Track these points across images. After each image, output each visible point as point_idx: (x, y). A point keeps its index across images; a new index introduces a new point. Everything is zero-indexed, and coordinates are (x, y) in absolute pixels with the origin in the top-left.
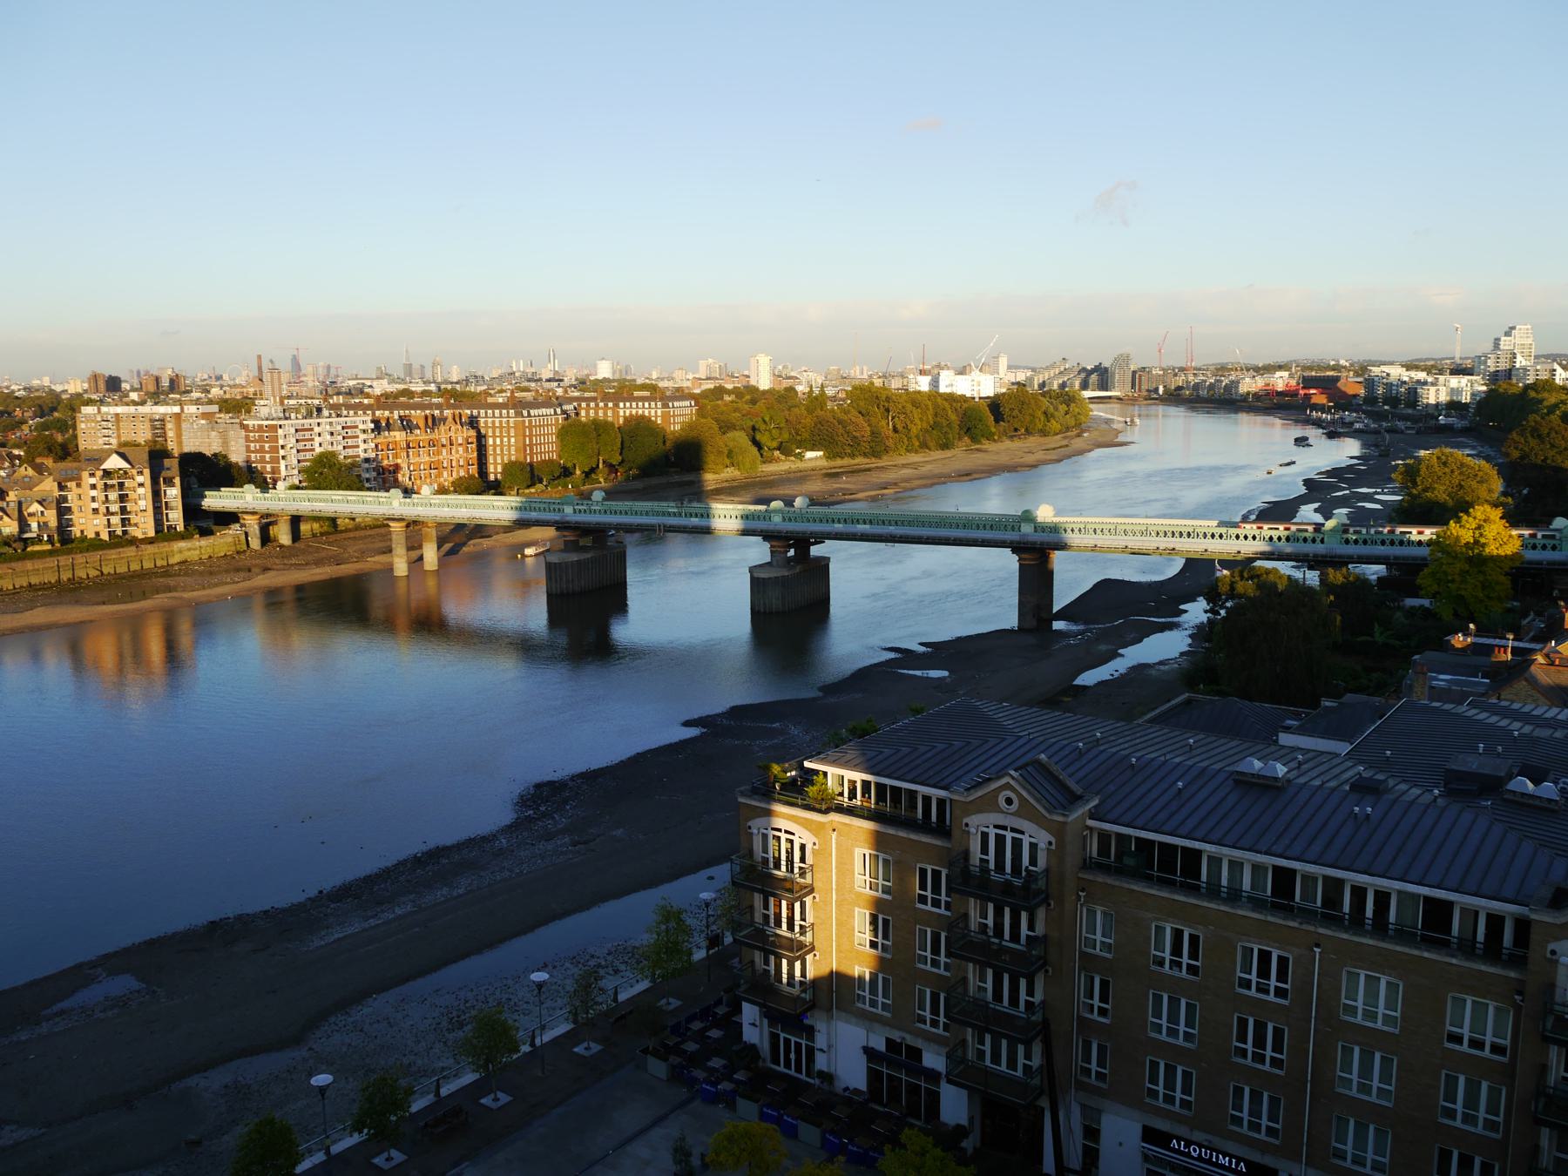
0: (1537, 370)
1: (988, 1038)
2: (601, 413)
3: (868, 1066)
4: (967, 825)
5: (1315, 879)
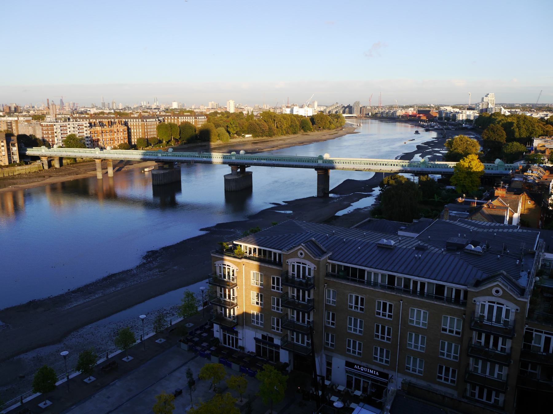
0: (496, 109)
1: (295, 333)
2: (172, 121)
3: (256, 344)
4: (287, 262)
5: (424, 283)
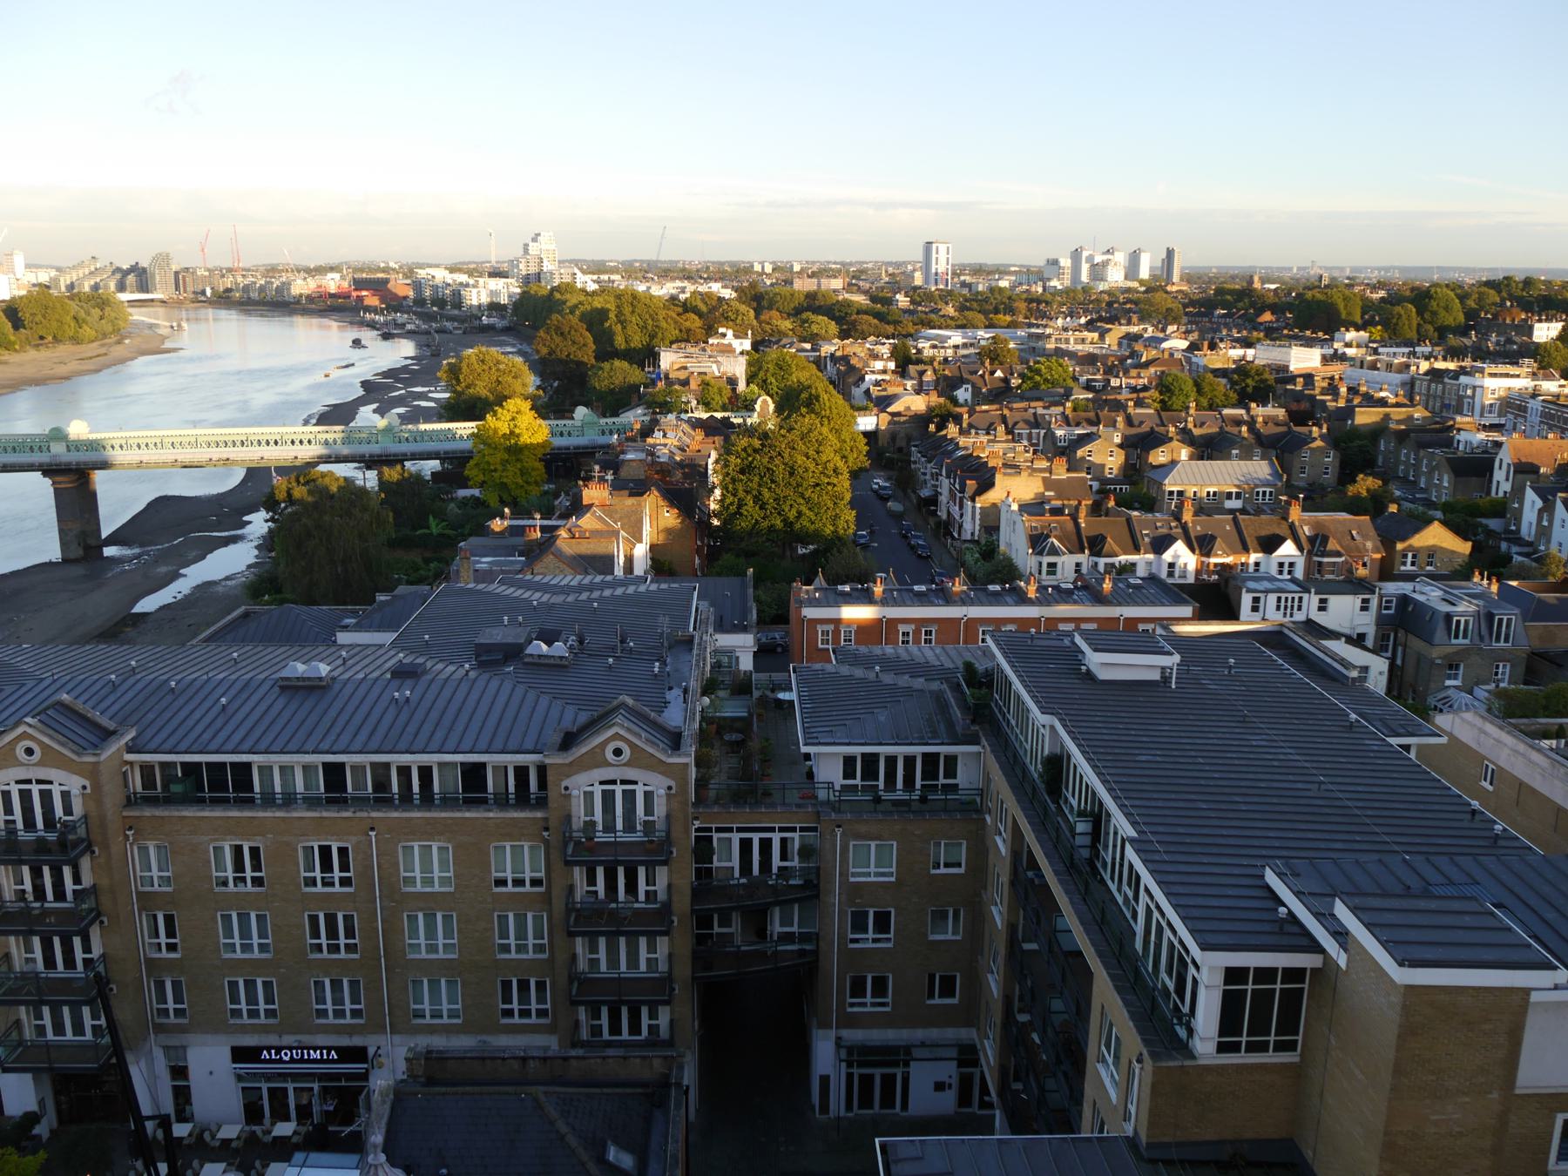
1: (46, 1010)
